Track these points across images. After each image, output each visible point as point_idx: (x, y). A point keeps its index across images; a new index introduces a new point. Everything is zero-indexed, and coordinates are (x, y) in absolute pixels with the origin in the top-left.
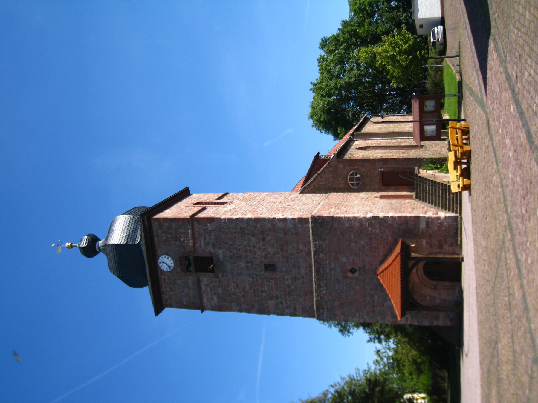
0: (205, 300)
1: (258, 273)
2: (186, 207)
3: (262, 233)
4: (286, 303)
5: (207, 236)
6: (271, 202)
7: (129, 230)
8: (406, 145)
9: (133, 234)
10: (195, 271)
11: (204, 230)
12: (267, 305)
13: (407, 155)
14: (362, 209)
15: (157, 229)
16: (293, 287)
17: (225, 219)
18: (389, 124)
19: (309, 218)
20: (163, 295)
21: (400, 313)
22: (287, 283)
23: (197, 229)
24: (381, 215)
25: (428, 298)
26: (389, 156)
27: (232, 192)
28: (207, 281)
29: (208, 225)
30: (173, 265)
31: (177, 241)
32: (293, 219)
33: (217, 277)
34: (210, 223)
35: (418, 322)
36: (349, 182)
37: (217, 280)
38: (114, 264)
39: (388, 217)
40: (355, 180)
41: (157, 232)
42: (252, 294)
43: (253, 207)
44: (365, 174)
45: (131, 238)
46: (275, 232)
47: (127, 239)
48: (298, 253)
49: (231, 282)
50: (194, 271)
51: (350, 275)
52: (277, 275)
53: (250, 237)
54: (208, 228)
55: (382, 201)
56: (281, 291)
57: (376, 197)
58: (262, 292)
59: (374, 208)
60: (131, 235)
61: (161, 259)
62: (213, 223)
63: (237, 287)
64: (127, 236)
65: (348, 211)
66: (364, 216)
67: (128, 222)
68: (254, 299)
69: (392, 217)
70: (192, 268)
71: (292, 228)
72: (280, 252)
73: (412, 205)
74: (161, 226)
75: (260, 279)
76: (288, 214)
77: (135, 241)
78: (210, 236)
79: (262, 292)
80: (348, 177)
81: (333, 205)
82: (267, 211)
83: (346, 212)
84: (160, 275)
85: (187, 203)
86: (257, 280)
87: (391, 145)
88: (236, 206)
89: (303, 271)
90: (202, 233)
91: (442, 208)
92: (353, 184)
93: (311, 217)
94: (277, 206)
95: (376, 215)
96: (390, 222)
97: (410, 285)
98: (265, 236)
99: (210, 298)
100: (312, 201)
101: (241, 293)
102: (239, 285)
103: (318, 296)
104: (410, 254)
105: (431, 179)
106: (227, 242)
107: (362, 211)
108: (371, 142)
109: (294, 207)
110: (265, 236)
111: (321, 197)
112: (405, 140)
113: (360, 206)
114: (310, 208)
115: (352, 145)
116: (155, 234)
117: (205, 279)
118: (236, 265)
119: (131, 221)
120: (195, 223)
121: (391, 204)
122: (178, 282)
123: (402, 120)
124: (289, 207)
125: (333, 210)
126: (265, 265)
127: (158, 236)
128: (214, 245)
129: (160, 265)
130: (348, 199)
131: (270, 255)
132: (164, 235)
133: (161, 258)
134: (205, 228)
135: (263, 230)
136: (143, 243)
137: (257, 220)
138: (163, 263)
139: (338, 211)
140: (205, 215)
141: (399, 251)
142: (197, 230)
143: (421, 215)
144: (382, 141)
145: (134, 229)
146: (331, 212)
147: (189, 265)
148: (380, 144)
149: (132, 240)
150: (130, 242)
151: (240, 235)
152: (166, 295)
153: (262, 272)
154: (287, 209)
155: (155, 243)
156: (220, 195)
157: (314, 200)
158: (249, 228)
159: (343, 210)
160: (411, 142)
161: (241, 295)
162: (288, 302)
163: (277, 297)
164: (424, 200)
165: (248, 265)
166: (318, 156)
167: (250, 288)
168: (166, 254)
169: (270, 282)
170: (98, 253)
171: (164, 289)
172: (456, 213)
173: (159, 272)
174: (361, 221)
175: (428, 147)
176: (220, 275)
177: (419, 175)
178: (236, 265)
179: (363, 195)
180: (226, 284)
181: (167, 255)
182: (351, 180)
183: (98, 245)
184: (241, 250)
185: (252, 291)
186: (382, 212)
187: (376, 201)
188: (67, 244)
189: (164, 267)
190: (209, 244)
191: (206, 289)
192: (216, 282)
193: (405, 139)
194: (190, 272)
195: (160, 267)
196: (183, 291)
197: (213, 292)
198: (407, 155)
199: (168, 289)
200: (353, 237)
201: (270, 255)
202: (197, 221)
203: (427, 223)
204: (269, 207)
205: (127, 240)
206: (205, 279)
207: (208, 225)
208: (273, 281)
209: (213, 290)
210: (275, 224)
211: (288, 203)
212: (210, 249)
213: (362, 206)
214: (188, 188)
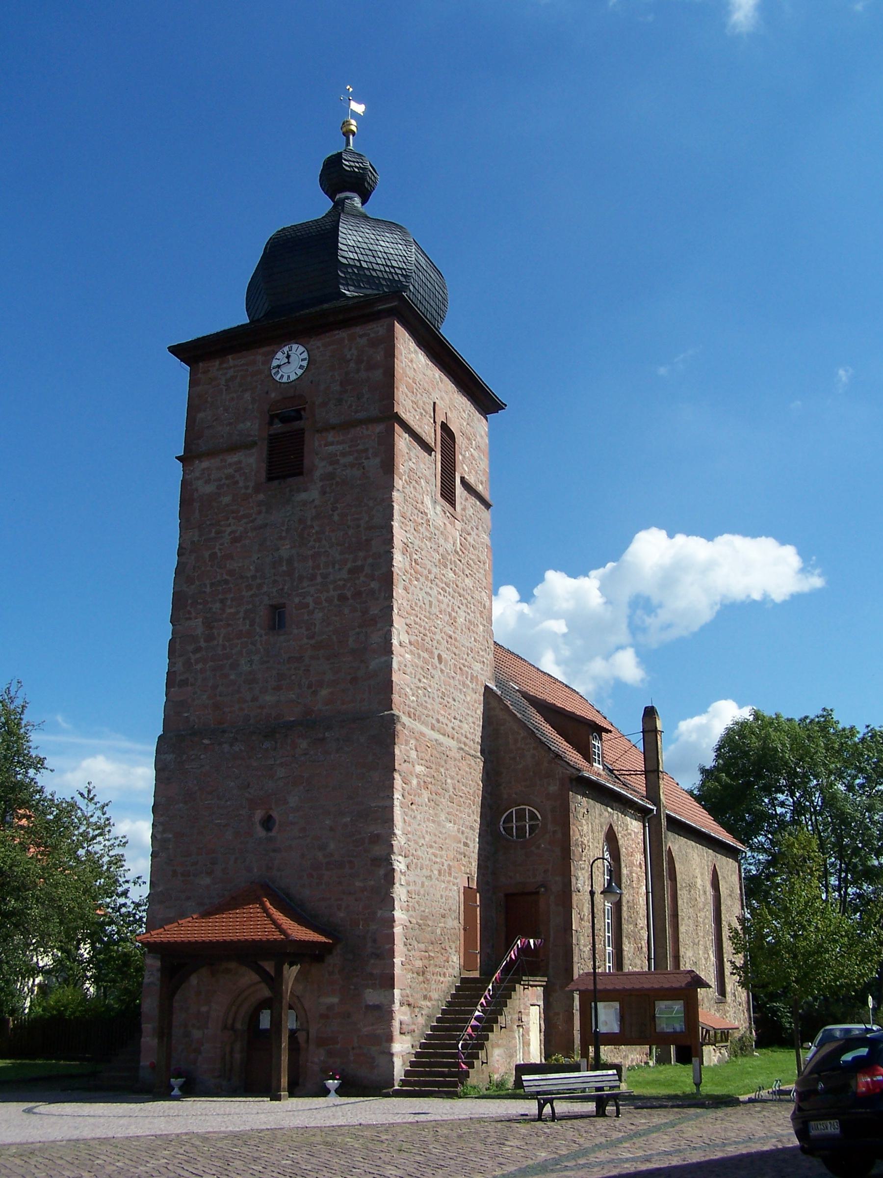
0: (205, 464)
1: (265, 589)
2: (434, 403)
3: (358, 594)
4: (197, 661)
5: (350, 459)
7: (376, 267)
10: (270, 435)
11: (366, 450)
12: (194, 614)
14: (422, 841)
16: (232, 677)
20: (217, 363)
25: (204, 1009)
27: (492, 519)
33: (257, 489)
37: (250, 491)
39: (394, 909)
41: (361, 336)
42: (219, 578)
43: (434, 570)
44: (533, 848)
48: (310, 687)
49: (247, 523)
50: (272, 432)
51: (259, 814)
52: (261, 636)
53: (349, 565)
54: (369, 458)
56: (224, 647)
63: (235, 540)
65: (414, 807)
66: (396, 849)
70: (278, 427)
71: (367, 667)
72: (313, 642)
75: (252, 596)
77: (347, 285)
78: (352, 466)
79: (222, 601)
80: (528, 807)
81: (437, 771)
82: (420, 603)
84: (264, 350)
85: (452, 407)
86: (249, 587)
87: (625, 915)
90: (359, 444)
91: (422, 1046)
92: (509, 819)
94: (438, 631)
97: (233, 965)
98: (351, 601)
99: (209, 475)
101: (220, 549)
102: (238, 545)
106: (337, 508)
107: (416, 843)
109: (437, 673)
110: (351, 601)
112: (645, 949)
113: (434, 838)
114: (431, 713)
117: (252, 460)
118: (284, 534)
119: (399, 271)
120: (380, 428)
122: (247, 396)
124: (436, 661)
125: (419, 769)
126: (283, 606)
128: (330, 476)
131: (306, 617)
133: (301, 349)
134: (371, 451)
135: (364, 595)
136: (342, 303)
137: (387, 581)
140: (406, 450)
142: (365, 432)
143: (397, 992)
146: (410, 766)
147: (285, 419)
152: (218, 370)
154: (426, 655)
156: (480, 488)
157: (461, 721)
159: (420, 795)
161: (217, 550)
162: (199, 667)
163: (209, 638)
165: (284, 564)
166: (599, 730)
167: (231, 573)
169: (244, 619)
170: (332, 197)
171: (231, 363)
172: (404, 1083)
176: (261, 497)
178: (284, 534)
180: (241, 513)
182: (521, 815)
183: (347, 198)
184: (317, 545)
190: (331, 464)
191: (230, 464)
192: (247, 488)
194: (271, 423)
196: (226, 410)
197: (223, 481)
199: (231, 373)
200: (345, 820)
203: (378, 1007)
204: (434, 610)
209: (227, 482)
210: (379, 625)
211: (449, 658)
212: (321, 468)
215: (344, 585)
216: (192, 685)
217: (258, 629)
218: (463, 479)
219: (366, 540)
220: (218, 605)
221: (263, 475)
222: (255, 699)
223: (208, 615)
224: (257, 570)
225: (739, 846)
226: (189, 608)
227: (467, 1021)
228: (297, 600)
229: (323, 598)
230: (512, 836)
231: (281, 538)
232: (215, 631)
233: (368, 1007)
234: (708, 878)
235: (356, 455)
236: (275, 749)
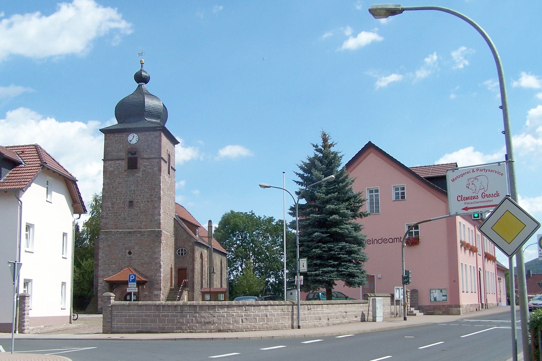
0: (110, 162)
1: (128, 197)
4: (110, 213)
5: (150, 167)
13: (196, 283)
16: (120, 218)
17: (160, 179)
18: (220, 270)
19: (160, 229)
21: (108, 280)
22: (122, 214)
24: (162, 270)
26: (196, 273)
28: (122, 164)
29: (157, 168)
30: (132, 143)
31: (147, 147)
32: (160, 220)
33: (125, 171)
34: (158, 169)
35: (100, 290)
41: (152, 135)
45: (149, 114)
46: (153, 209)
50: (129, 157)
51: (128, 251)
53: (150, 193)
55: (169, 269)
56: (117, 210)
57: (172, 265)
58: (116, 199)
59: (165, 265)
61: (136, 135)
62: (158, 171)
63: (119, 184)
64: (149, 111)
68: (112, 193)
69: (161, 276)
70: (130, 155)
73: (167, 287)
74: (156, 137)
76: (163, 215)
79: (116, 199)
80: (184, 248)
84: (125, 133)
86: (123, 196)
88: (167, 182)
89: (129, 224)
96: (158, 275)
98: (150, 202)
99: (111, 165)
102: (120, 185)
103: (114, 232)
104: (140, 285)
105: (182, 298)
108: (206, 261)
110: (150, 202)
112: (207, 282)
115: (204, 249)
116: (152, 133)
117: (123, 163)
118: (132, 184)
119: (159, 113)
120: (157, 160)
121: (168, 274)
122: (121, 146)
123: (223, 279)
125: (165, 241)
128: (144, 171)
129: (132, 134)
131: (139, 205)
132: (151, 139)
133: (136, 135)
134: (155, 166)
137: (160, 198)
138: (133, 137)
139: (164, 245)
141: (143, 280)
144: (207, 267)
150: (146, 113)
151: (151, 187)
152: (113, 137)
153: (128, 199)
154: (165, 214)
158: (155, 193)
160: (205, 286)
161: (114, 185)
164: (170, 293)
167: (118, 192)
169: (122, 204)
171: (116, 135)
174: (159, 258)
176: (126, 173)
177: (184, 291)
178: (132, 184)
179: (173, 257)
182: (182, 250)
183: (143, 84)
184: (141, 187)
185: (117, 192)
186: (163, 270)
189: (130, 137)
191: (117, 164)
195: (130, 134)
198: (196, 283)
201: (139, 205)
203: (157, 295)
205: (148, 112)
206: (124, 164)
207: (157, 168)
208: (123, 206)
209: (116, 168)
210: (157, 209)
212: (142, 168)
215: (148, 198)
216: (108, 219)
217: (126, 207)
218: (171, 167)
219: (154, 188)
220: (115, 200)
221: (127, 168)
222: (125, 224)
223: (112, 202)
224: (125, 192)
225: (225, 252)
226: (107, 199)
227: (177, 298)
228: (136, 201)
229: (143, 201)
230: (180, 255)
231: (132, 185)
232: (115, 206)
233: (155, 295)
234: (220, 262)
235: (151, 166)
236: (131, 236)
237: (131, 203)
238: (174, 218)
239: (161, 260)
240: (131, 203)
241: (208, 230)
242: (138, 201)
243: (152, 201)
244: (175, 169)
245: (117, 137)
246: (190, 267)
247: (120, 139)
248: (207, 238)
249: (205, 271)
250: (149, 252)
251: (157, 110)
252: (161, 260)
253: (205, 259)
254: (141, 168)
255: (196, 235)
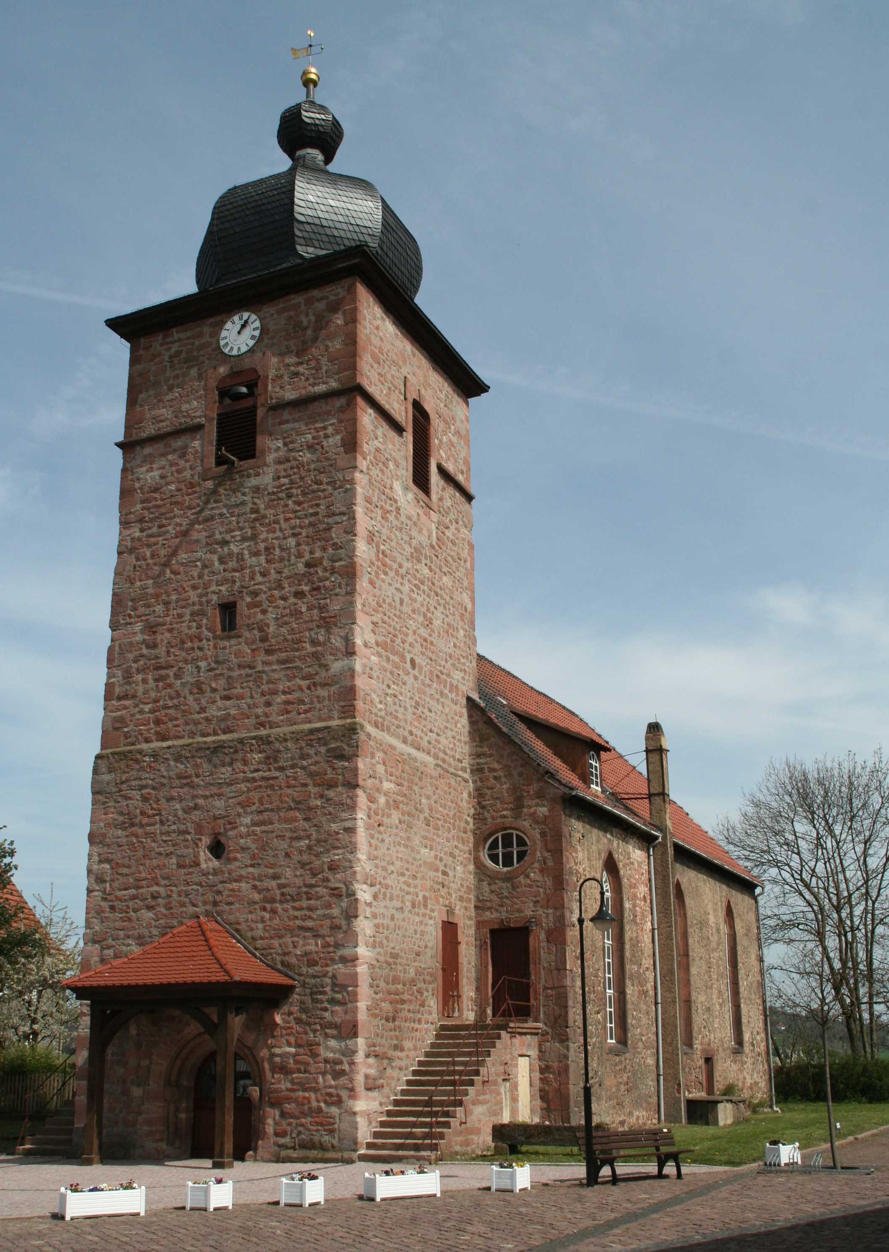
6: (429, 615)
7: (338, 225)
8: (628, 997)
9: (325, 239)
15: (327, 298)
23: (329, 408)
29: (338, 437)
34: (344, 444)
36: (500, 835)
38: (360, 241)
40: (521, 849)
41: (319, 300)
43: (406, 565)
47: (310, 220)
59: (398, 904)
60: (321, 231)
64: (317, 222)
65: (381, 828)
67: (359, 222)
79: (167, 604)
80: (515, 832)
83: (379, 825)
93: (355, 723)
95: (364, 911)
100: (435, 730)
104: (238, 1012)
111: (453, 757)
112: (651, 993)
116: (316, 293)
119: (364, 230)
123: (743, 984)
127: (309, 302)
129: (236, 318)
130: (440, 833)
145: (338, 240)
148: (634, 921)
149: (306, 235)
152: (161, 345)
155: (292, 296)
168: (264, 330)
171: (176, 336)
173: (218, 318)
175: (617, 1059)
181: (261, 334)
187: (432, 910)
188: (313, 70)
193: (656, 994)
199: (175, 347)
202: (348, 405)
205: (308, 223)
207: (338, 437)
213: (407, 869)
214: (487, 391)
237: (228, 610)
238: (469, 699)
239: (355, 873)
240: (228, 610)
241: (645, 773)
242: (258, 599)
243: (318, 589)
244: (473, 491)
245: (180, 340)
246: (546, 917)
247: (189, 347)
248: (647, 801)
249: (636, 943)
250: (299, 838)
251: (351, 218)
252: (359, 877)
253: (634, 886)
254: (269, 449)
255: (586, 779)
